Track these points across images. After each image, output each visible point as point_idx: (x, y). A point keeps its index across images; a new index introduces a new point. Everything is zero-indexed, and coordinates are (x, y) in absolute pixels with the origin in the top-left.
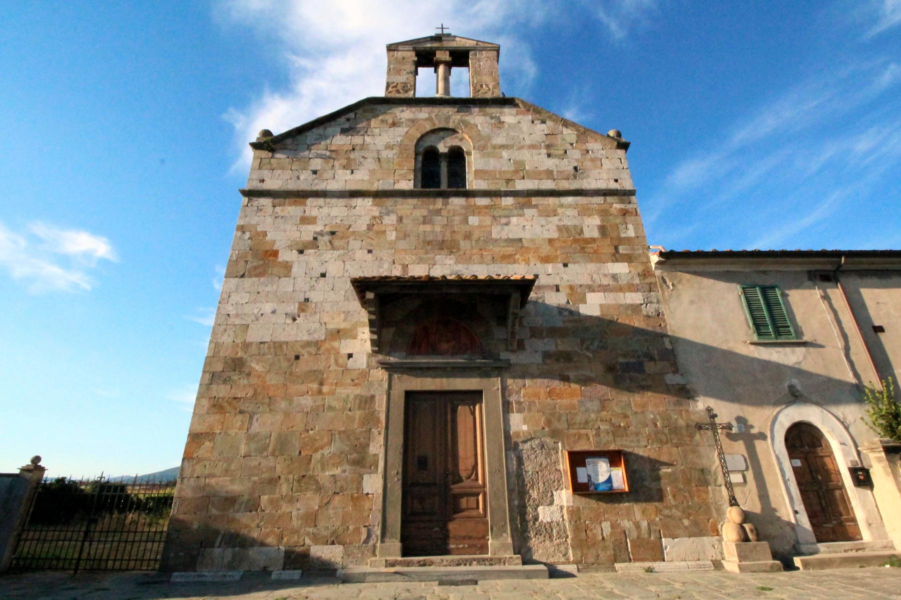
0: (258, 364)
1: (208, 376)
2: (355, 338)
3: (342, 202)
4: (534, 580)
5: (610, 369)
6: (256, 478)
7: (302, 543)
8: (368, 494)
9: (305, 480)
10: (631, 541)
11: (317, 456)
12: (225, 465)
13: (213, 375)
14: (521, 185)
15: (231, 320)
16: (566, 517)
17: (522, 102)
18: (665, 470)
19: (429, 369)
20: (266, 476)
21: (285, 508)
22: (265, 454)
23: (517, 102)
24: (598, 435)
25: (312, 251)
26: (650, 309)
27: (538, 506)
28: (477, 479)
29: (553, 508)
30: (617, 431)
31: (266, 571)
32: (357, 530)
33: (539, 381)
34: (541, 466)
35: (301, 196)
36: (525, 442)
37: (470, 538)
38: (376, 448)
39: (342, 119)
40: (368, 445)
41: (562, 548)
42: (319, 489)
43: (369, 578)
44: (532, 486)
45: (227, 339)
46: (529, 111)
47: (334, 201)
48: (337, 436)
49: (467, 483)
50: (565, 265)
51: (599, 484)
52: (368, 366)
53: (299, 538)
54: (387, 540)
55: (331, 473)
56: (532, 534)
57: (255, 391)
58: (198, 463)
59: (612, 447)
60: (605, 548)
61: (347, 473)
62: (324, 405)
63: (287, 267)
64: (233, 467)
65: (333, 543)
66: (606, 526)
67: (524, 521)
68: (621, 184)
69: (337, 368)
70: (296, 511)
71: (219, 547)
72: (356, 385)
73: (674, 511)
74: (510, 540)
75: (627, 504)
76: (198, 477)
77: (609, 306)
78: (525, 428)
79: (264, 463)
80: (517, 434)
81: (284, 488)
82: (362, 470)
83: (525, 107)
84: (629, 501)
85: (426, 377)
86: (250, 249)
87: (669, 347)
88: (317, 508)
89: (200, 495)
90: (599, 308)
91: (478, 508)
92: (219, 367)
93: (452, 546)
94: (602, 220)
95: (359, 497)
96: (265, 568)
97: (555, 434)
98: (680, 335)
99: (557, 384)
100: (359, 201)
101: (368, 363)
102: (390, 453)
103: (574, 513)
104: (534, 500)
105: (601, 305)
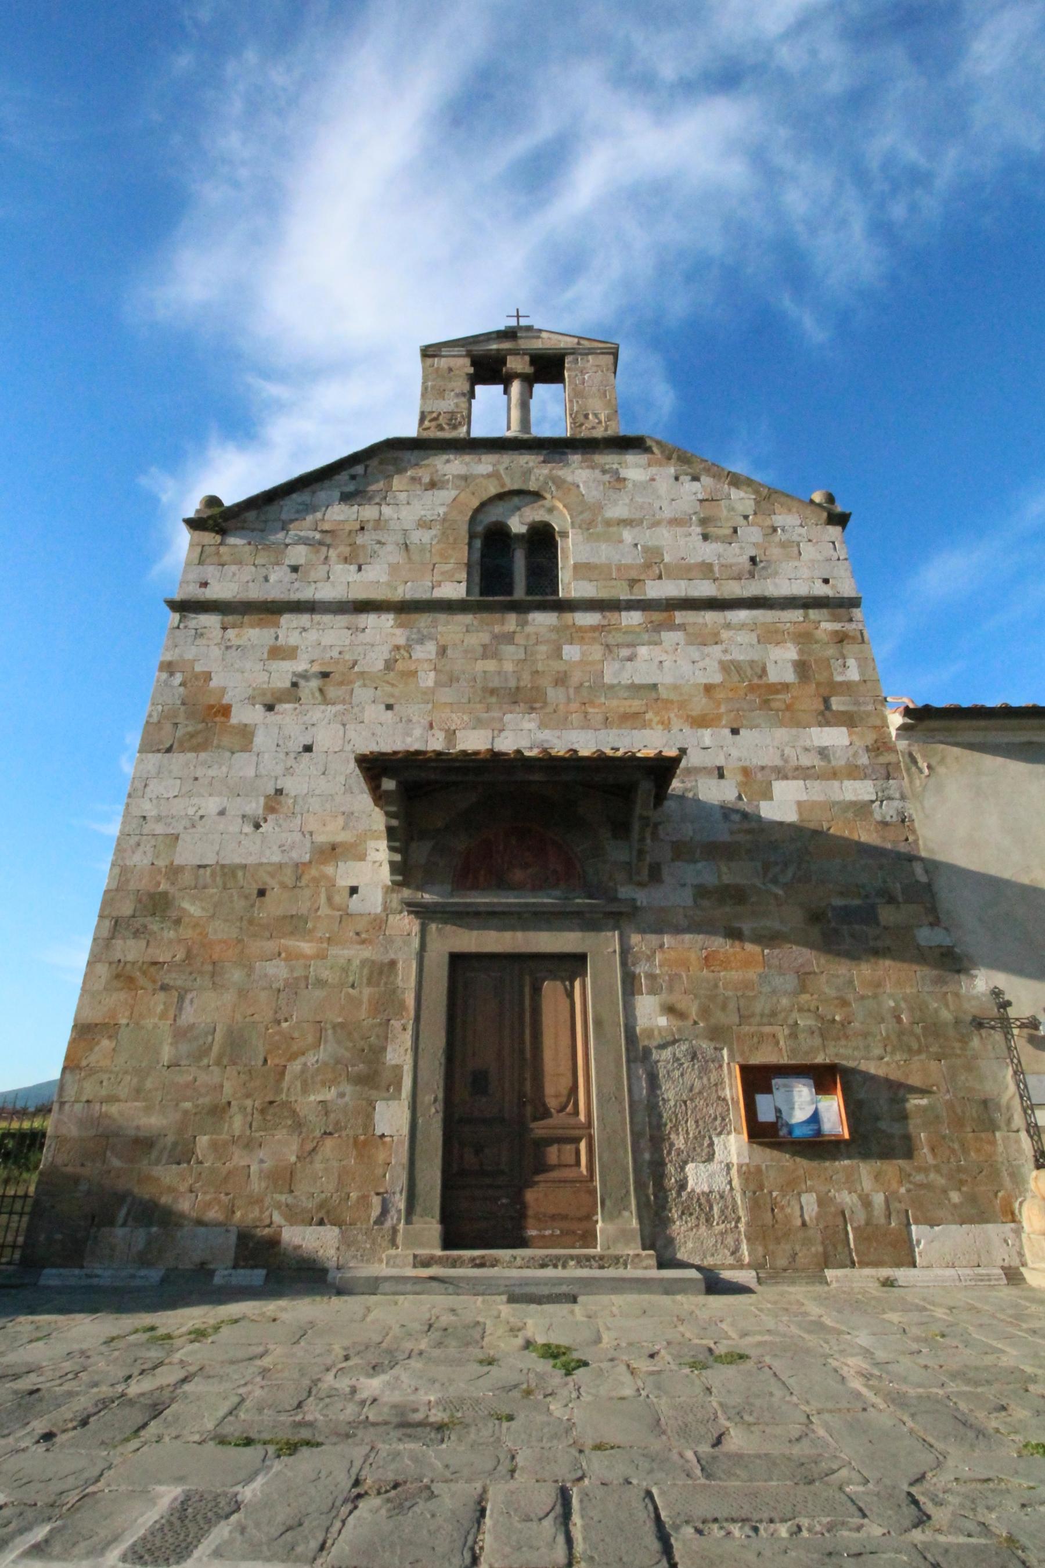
0: (193, 904)
1: (107, 924)
2: (362, 857)
5: (815, 917)
6: (188, 1105)
8: (383, 1136)
9: (273, 1110)
12: (135, 1080)
14: (654, 590)
16: (736, 1183)
18: (916, 1102)
21: (239, 1158)
23: (649, 443)
24: (793, 1035)
25: (288, 706)
26: (888, 811)
28: (576, 1113)
29: (714, 1166)
30: (827, 1030)
31: (203, 1271)
32: (364, 1199)
35: (271, 610)
36: (662, 1047)
37: (564, 1217)
38: (398, 1054)
39: (344, 476)
40: (384, 1049)
41: (730, 1240)
42: (298, 1125)
44: (676, 1127)
45: (140, 860)
46: (669, 458)
47: (327, 618)
49: (557, 1119)
50: (735, 732)
53: (262, 1212)
54: (415, 1218)
55: (320, 1098)
56: (675, 1214)
59: (819, 1059)
61: (347, 1098)
62: (307, 978)
64: (149, 1084)
65: (321, 1223)
66: (809, 1200)
70: (257, 1163)
72: (363, 942)
74: (635, 1223)
76: (88, 1101)
77: (814, 805)
79: (203, 1078)
80: (649, 1033)
81: (237, 1123)
82: (374, 1093)
83: (662, 452)
86: (183, 704)
87: (923, 879)
90: (794, 808)
91: (578, 1163)
92: (126, 909)
93: (532, 1232)
95: (367, 1142)
99: (719, 944)
104: (679, 1152)
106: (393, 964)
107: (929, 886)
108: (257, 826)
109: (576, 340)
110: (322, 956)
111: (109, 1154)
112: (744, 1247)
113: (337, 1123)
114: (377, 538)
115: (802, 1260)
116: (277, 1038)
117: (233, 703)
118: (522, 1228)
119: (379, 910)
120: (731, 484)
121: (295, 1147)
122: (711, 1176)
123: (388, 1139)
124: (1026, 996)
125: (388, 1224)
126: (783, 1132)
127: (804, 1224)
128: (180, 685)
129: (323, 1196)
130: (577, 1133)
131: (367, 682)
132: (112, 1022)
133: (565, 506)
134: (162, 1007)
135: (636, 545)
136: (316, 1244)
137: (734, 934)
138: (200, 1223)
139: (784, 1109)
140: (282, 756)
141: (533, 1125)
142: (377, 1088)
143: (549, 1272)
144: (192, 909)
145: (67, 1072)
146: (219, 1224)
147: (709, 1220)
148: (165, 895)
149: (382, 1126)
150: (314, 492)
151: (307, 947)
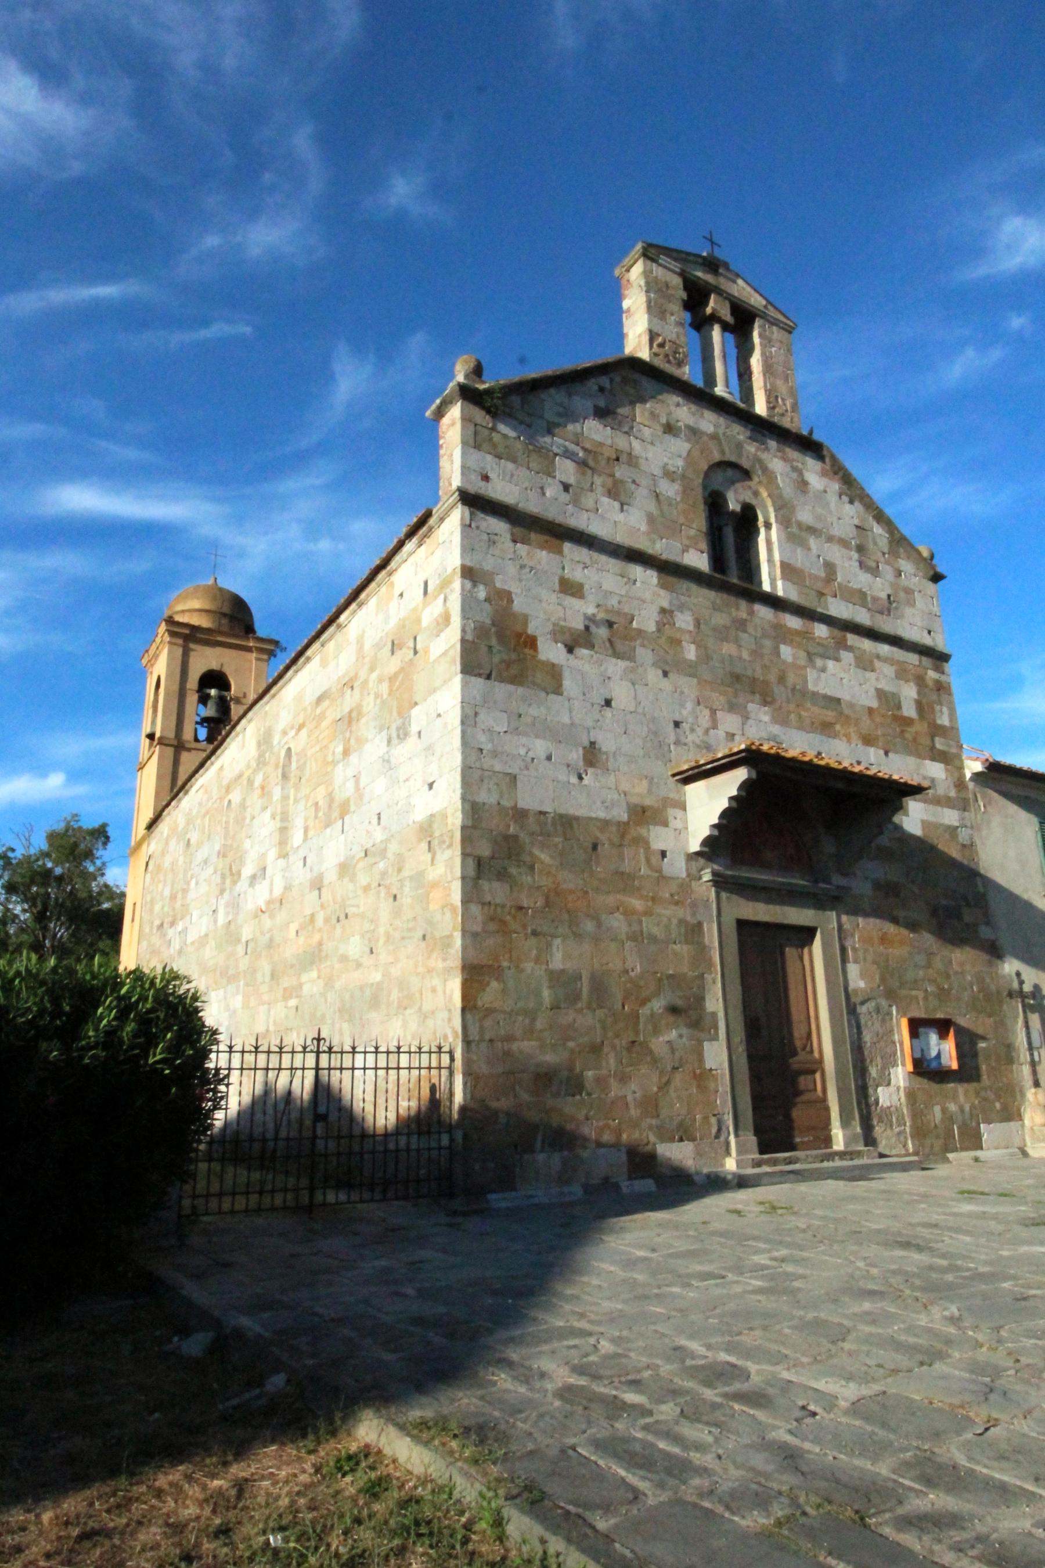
0: (542, 851)
2: (666, 824)
3: (613, 564)
4: (912, 1173)
5: (934, 912)
7: (645, 1141)
8: (711, 1070)
10: (958, 1128)
11: (645, 1011)
12: (527, 1021)
13: (479, 863)
15: (488, 762)
16: (903, 1099)
17: (833, 457)
18: (982, 1045)
19: (764, 889)
20: (585, 1040)
21: (615, 1090)
22: (579, 1005)
23: (825, 452)
26: (963, 835)
27: (877, 1086)
28: (812, 1051)
29: (892, 1089)
30: (943, 995)
31: (608, 1185)
32: (706, 1118)
33: (872, 920)
34: (878, 1035)
36: (863, 1003)
37: (814, 1128)
38: (714, 1003)
39: (592, 384)
40: (703, 998)
41: (902, 1139)
42: (655, 1061)
43: (765, 1180)
44: (871, 1061)
46: (836, 473)
47: (603, 558)
48: (666, 982)
49: (802, 1056)
50: (886, 753)
51: (931, 1059)
52: (688, 875)
53: (641, 1134)
54: (740, 1133)
55: (667, 1038)
56: (875, 1122)
57: (547, 897)
58: (486, 1016)
59: (940, 1015)
60: (937, 1137)
61: (684, 1039)
62: (642, 932)
63: (554, 673)
64: (539, 1024)
65: (681, 1140)
66: (937, 1109)
67: (868, 1105)
68: (934, 639)
69: (649, 873)
70: (633, 1091)
71: (542, 1151)
72: (677, 903)
73: (989, 1092)
74: (859, 1130)
75: (952, 1085)
76: (491, 1041)
77: (937, 826)
78: (862, 984)
80: (855, 991)
81: (611, 1061)
82: (702, 1035)
83: (833, 466)
84: (953, 1081)
85: (757, 900)
86: (493, 624)
87: (982, 890)
88: (655, 1089)
89: (500, 1070)
90: (919, 825)
91: (815, 1090)
92: (485, 850)
93: (798, 1140)
94: (919, 693)
95: (703, 1077)
96: (606, 1179)
97: (891, 995)
98: (990, 875)
99: (891, 929)
100: (638, 571)
101: (687, 870)
102: (730, 1011)
103: (911, 1095)
104: (874, 1079)
105: (923, 822)
106: (700, 924)
107: (984, 895)
108: (580, 778)
109: (764, 302)
110: (648, 913)
111: (517, 1087)
112: (910, 1142)
113: (681, 1059)
114: (634, 477)
115: (936, 1149)
116: (629, 985)
117: (537, 633)
118: (791, 1137)
119: (684, 875)
120: (874, 517)
121: (655, 1080)
122: (890, 1095)
123: (714, 1072)
124: (1032, 977)
125: (722, 1139)
126: (925, 1064)
127: (936, 1125)
128: (485, 600)
129: (680, 1118)
130: (814, 1067)
131: (645, 642)
132: (496, 965)
133: (769, 495)
134: (535, 952)
135: (819, 556)
136: (680, 1157)
137: (895, 920)
138: (599, 1145)
139: (925, 1048)
140: (588, 705)
141: (791, 1061)
142: (702, 1031)
143: (825, 1164)
144: (543, 856)
145: (467, 1012)
146: (612, 1146)
147: (891, 1126)
148: (515, 837)
149: (709, 1064)
150: (570, 395)
151: (637, 904)
